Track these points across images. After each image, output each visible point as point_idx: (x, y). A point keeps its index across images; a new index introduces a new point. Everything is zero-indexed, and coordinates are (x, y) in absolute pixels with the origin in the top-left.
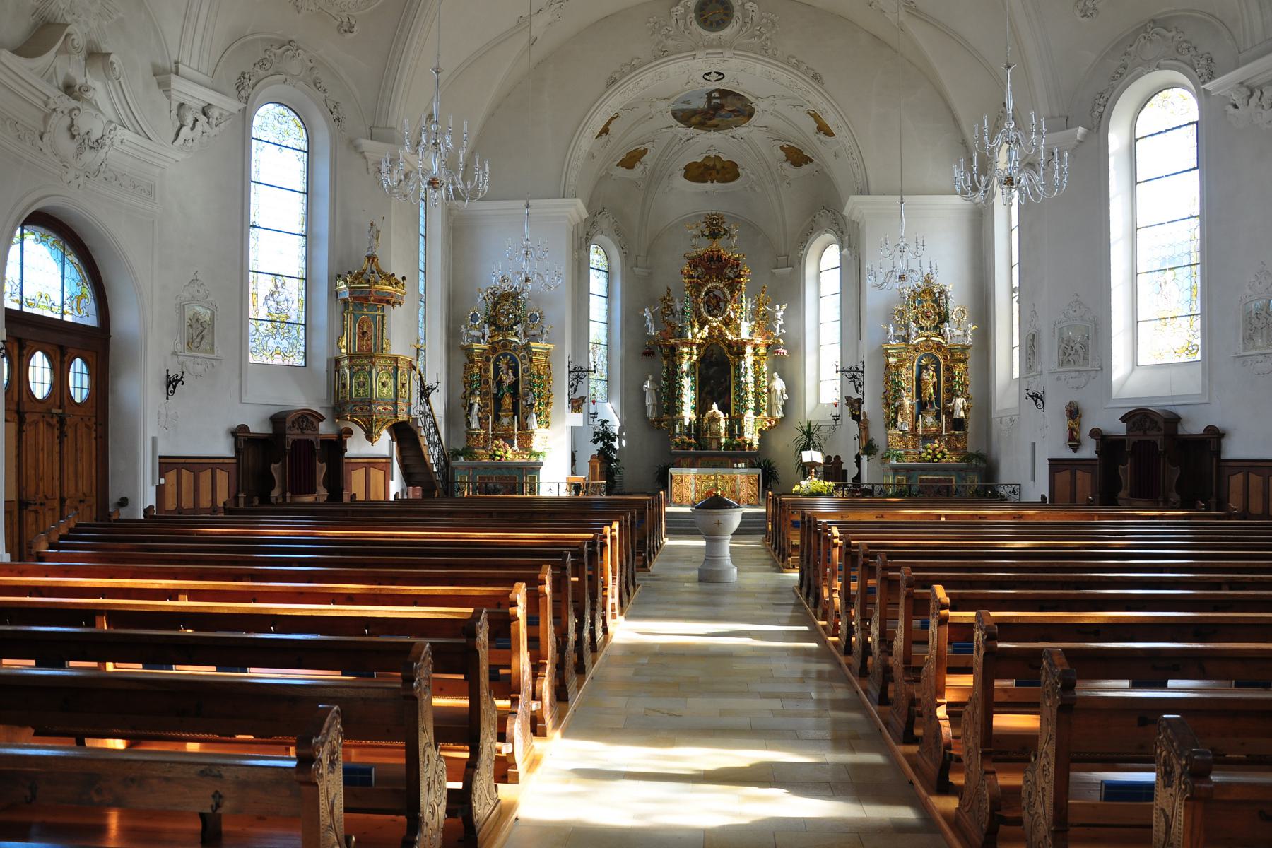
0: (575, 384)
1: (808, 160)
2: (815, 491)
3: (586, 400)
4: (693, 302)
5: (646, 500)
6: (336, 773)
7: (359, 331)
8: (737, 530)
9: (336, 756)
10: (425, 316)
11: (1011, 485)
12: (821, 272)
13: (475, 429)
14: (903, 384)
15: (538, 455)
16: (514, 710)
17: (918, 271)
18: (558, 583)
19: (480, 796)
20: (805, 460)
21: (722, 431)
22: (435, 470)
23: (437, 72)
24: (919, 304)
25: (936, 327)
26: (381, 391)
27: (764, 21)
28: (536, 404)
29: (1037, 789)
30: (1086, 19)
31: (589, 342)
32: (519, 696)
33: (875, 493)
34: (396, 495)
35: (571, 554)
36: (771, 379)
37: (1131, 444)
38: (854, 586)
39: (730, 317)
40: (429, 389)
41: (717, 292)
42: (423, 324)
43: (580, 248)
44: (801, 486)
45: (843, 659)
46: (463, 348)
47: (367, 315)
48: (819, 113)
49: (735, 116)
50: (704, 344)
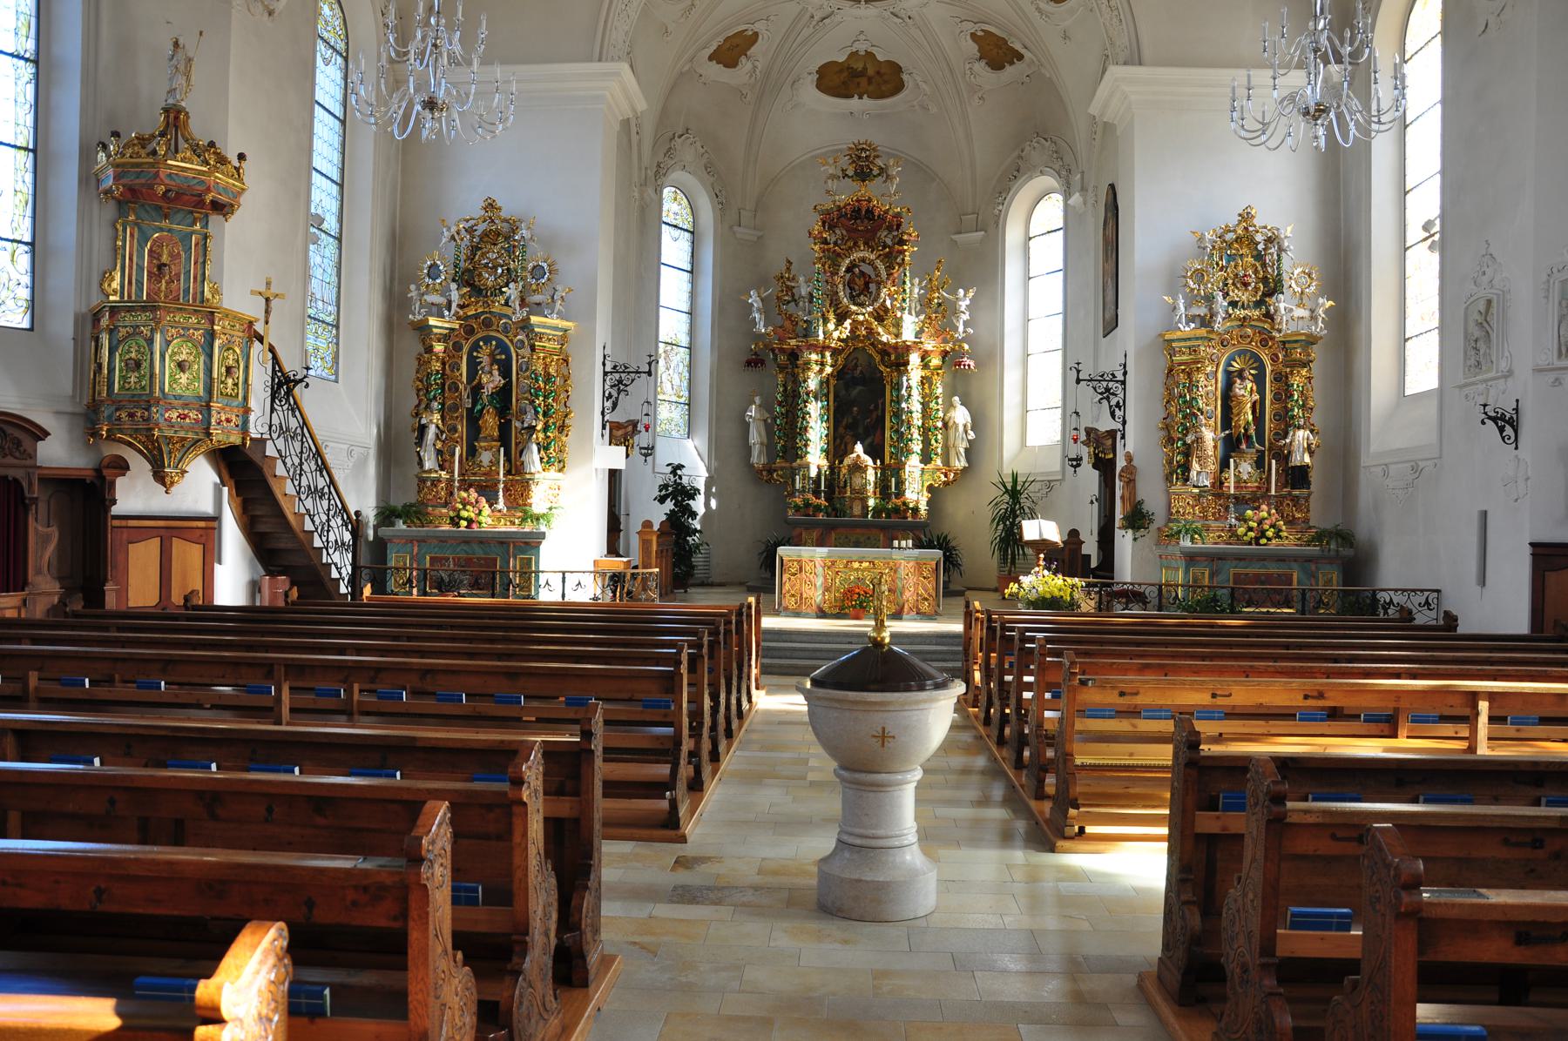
0: (615, 394)
4: (827, 282)
11: (1422, 591)
12: (1030, 239)
13: (430, 471)
14: (1200, 402)
15: (538, 519)
21: (870, 488)
24: (1228, 262)
25: (1258, 304)
26: (175, 381)
28: (539, 428)
31: (657, 341)
36: (949, 406)
39: (885, 307)
43: (644, 184)
44: (1020, 587)
50: (843, 350)
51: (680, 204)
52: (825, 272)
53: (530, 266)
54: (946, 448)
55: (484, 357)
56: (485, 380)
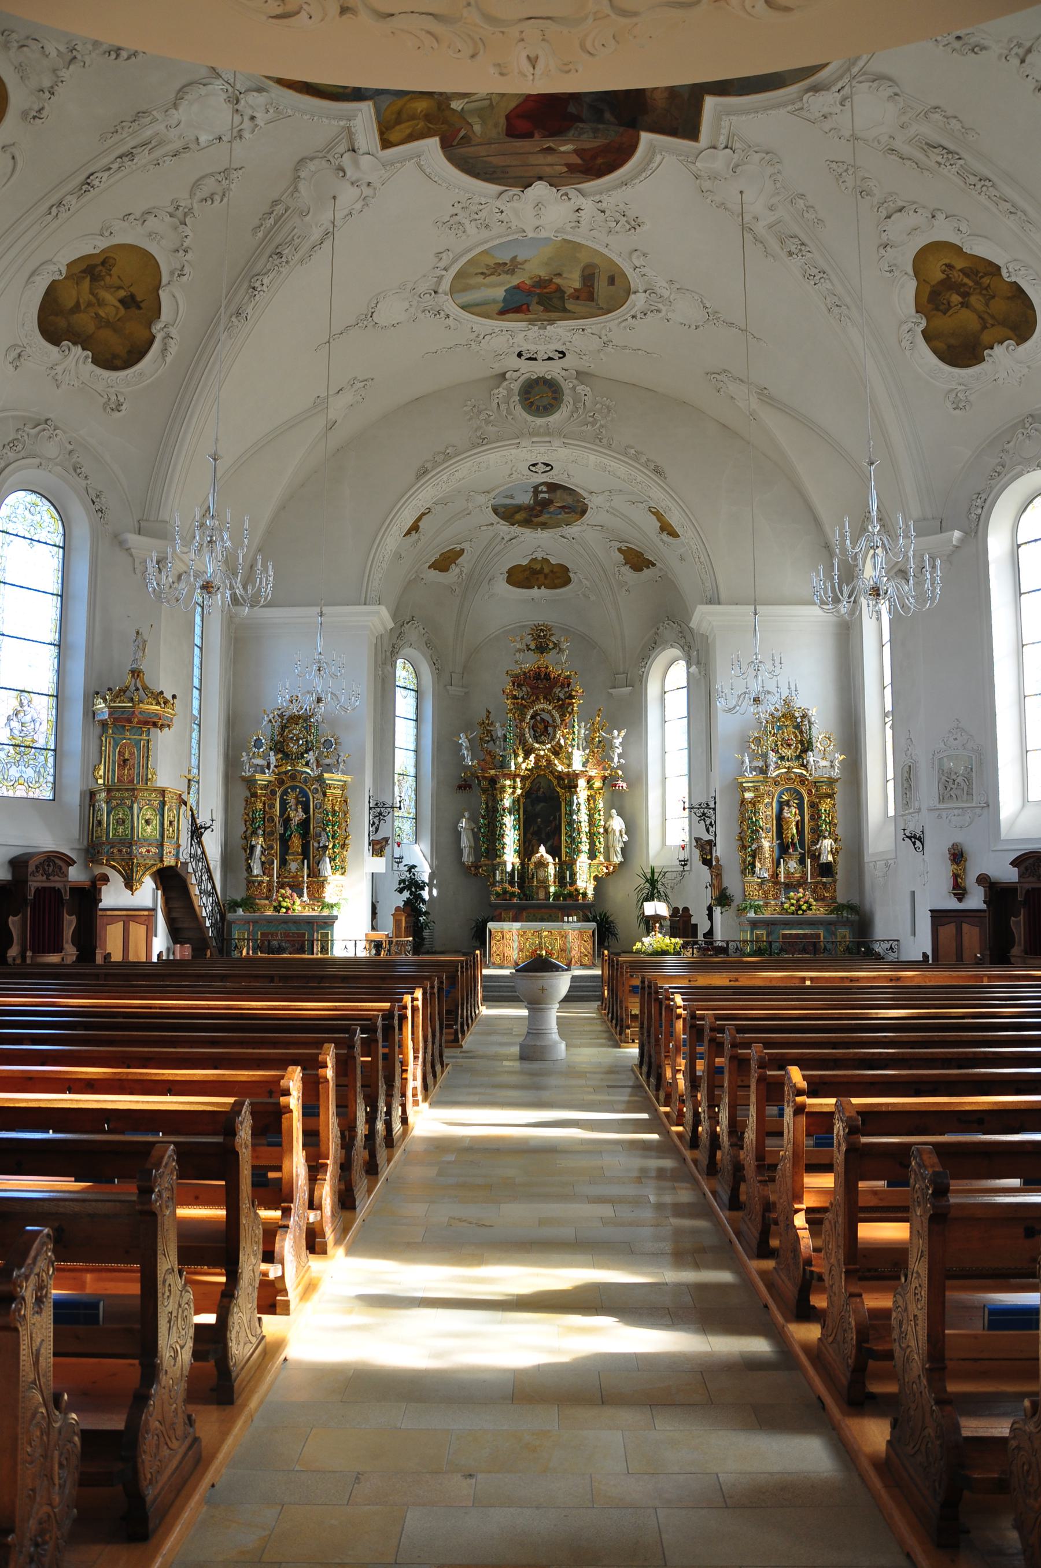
0: (377, 822)
1: (650, 564)
2: (659, 950)
3: (390, 842)
4: (517, 726)
5: (458, 961)
6: (44, 1314)
7: (119, 758)
8: (566, 996)
9: (44, 1292)
10: (199, 741)
11: (888, 941)
12: (665, 693)
13: (257, 876)
15: (332, 907)
16: (285, 1223)
17: (775, 693)
18: (344, 1066)
19: (238, 1333)
20: (647, 913)
21: (551, 879)
22: (208, 925)
23: (215, 460)
24: (778, 731)
25: (798, 757)
27: (598, 406)
28: (330, 846)
29: (908, 1316)
30: (958, 411)
31: (394, 774)
32: (292, 1205)
33: (730, 952)
34: (160, 955)
35: (361, 1030)
36: (608, 817)
37: (1024, 892)
38: (700, 1066)
39: (560, 744)
40: (201, 827)
41: (546, 716)
42: (197, 751)
43: (384, 663)
45: (688, 1154)
46: (243, 779)
47: (129, 739)
48: (661, 511)
49: (566, 513)
50: (530, 776)
51: (408, 671)
52: (515, 719)
53: (322, 740)
54: (607, 847)
55: (291, 800)
56: (292, 815)
